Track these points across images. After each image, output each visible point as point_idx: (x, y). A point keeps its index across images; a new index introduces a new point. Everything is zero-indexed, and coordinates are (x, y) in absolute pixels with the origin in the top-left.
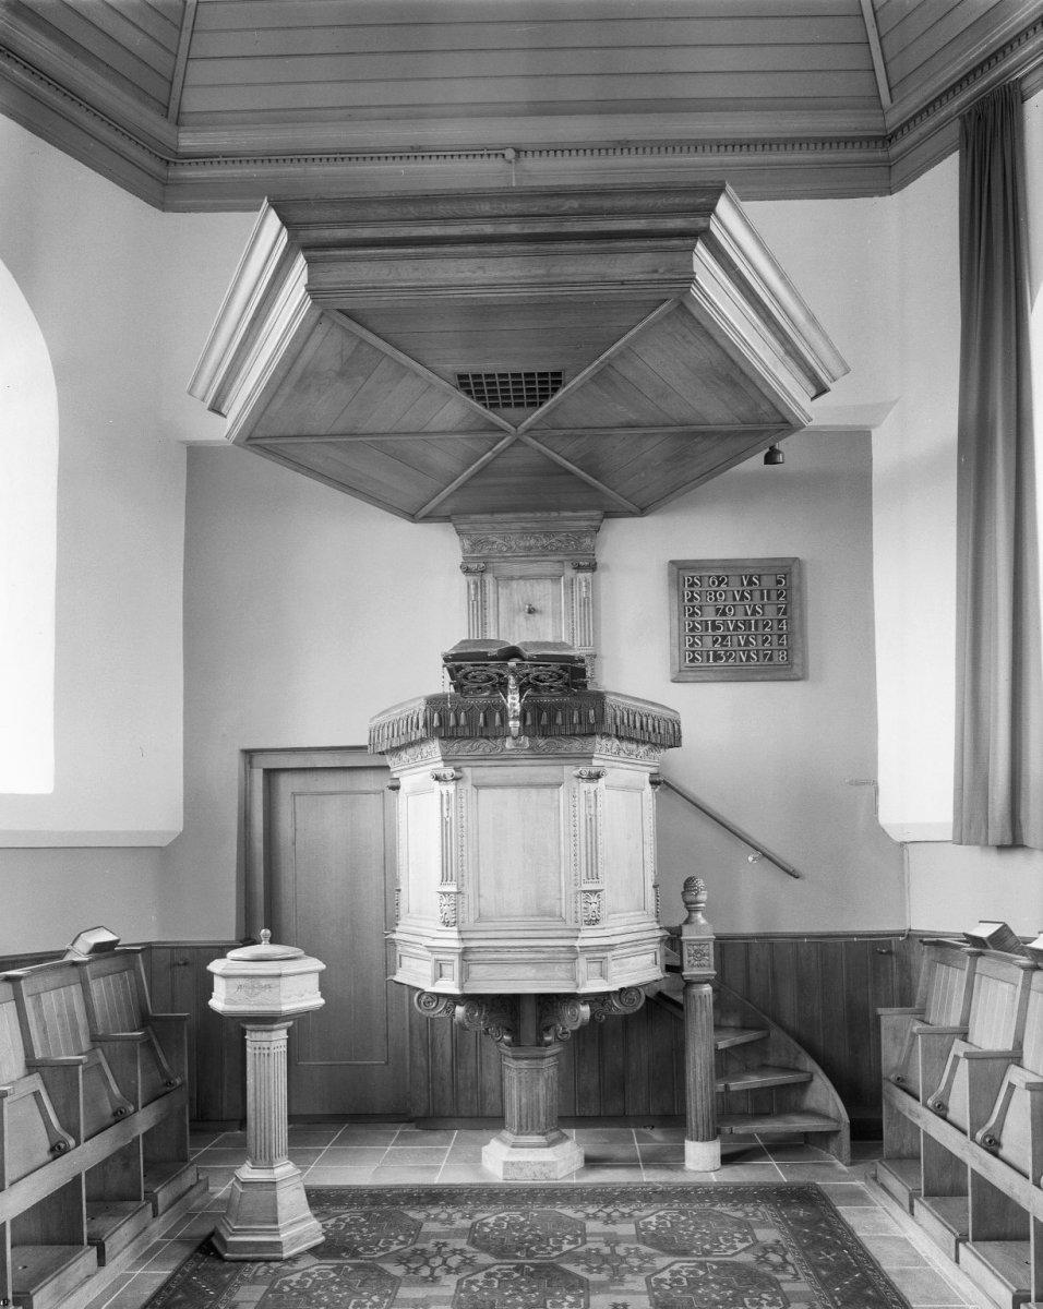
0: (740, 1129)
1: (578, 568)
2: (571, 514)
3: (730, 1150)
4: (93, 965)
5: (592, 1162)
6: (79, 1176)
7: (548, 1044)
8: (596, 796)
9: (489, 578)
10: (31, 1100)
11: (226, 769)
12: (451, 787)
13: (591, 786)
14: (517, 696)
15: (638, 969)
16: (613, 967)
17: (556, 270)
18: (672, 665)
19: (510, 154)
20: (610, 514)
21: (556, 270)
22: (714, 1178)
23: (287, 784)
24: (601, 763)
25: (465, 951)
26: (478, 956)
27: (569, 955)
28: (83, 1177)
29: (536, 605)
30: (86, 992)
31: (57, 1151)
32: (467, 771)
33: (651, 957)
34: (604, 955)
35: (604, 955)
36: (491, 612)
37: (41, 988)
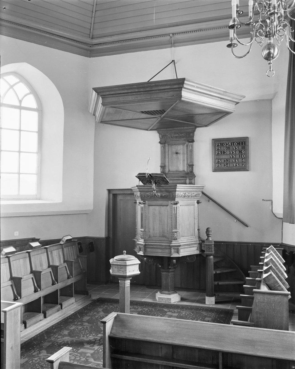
0: (221, 295)
1: (189, 142)
2: (187, 128)
3: (217, 301)
4: (65, 245)
5: (182, 299)
6: (58, 290)
7: (170, 268)
8: (177, 208)
9: (166, 145)
10: (49, 273)
11: (105, 195)
12: (143, 205)
13: (175, 206)
14: (154, 185)
15: (194, 251)
16: (181, 251)
17: (152, 97)
18: (213, 167)
19: (171, 35)
20: (196, 127)
21: (152, 97)
22: (214, 306)
23: (119, 198)
24: (178, 200)
25: (145, 245)
26: (148, 246)
27: (169, 247)
28: (59, 290)
29: (178, 152)
30: (63, 250)
31: (53, 284)
32: (147, 202)
33: (196, 248)
34: (178, 248)
35: (178, 248)
36: (167, 154)
37: (52, 250)
